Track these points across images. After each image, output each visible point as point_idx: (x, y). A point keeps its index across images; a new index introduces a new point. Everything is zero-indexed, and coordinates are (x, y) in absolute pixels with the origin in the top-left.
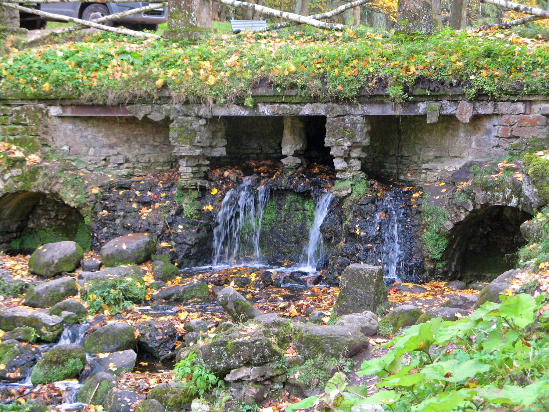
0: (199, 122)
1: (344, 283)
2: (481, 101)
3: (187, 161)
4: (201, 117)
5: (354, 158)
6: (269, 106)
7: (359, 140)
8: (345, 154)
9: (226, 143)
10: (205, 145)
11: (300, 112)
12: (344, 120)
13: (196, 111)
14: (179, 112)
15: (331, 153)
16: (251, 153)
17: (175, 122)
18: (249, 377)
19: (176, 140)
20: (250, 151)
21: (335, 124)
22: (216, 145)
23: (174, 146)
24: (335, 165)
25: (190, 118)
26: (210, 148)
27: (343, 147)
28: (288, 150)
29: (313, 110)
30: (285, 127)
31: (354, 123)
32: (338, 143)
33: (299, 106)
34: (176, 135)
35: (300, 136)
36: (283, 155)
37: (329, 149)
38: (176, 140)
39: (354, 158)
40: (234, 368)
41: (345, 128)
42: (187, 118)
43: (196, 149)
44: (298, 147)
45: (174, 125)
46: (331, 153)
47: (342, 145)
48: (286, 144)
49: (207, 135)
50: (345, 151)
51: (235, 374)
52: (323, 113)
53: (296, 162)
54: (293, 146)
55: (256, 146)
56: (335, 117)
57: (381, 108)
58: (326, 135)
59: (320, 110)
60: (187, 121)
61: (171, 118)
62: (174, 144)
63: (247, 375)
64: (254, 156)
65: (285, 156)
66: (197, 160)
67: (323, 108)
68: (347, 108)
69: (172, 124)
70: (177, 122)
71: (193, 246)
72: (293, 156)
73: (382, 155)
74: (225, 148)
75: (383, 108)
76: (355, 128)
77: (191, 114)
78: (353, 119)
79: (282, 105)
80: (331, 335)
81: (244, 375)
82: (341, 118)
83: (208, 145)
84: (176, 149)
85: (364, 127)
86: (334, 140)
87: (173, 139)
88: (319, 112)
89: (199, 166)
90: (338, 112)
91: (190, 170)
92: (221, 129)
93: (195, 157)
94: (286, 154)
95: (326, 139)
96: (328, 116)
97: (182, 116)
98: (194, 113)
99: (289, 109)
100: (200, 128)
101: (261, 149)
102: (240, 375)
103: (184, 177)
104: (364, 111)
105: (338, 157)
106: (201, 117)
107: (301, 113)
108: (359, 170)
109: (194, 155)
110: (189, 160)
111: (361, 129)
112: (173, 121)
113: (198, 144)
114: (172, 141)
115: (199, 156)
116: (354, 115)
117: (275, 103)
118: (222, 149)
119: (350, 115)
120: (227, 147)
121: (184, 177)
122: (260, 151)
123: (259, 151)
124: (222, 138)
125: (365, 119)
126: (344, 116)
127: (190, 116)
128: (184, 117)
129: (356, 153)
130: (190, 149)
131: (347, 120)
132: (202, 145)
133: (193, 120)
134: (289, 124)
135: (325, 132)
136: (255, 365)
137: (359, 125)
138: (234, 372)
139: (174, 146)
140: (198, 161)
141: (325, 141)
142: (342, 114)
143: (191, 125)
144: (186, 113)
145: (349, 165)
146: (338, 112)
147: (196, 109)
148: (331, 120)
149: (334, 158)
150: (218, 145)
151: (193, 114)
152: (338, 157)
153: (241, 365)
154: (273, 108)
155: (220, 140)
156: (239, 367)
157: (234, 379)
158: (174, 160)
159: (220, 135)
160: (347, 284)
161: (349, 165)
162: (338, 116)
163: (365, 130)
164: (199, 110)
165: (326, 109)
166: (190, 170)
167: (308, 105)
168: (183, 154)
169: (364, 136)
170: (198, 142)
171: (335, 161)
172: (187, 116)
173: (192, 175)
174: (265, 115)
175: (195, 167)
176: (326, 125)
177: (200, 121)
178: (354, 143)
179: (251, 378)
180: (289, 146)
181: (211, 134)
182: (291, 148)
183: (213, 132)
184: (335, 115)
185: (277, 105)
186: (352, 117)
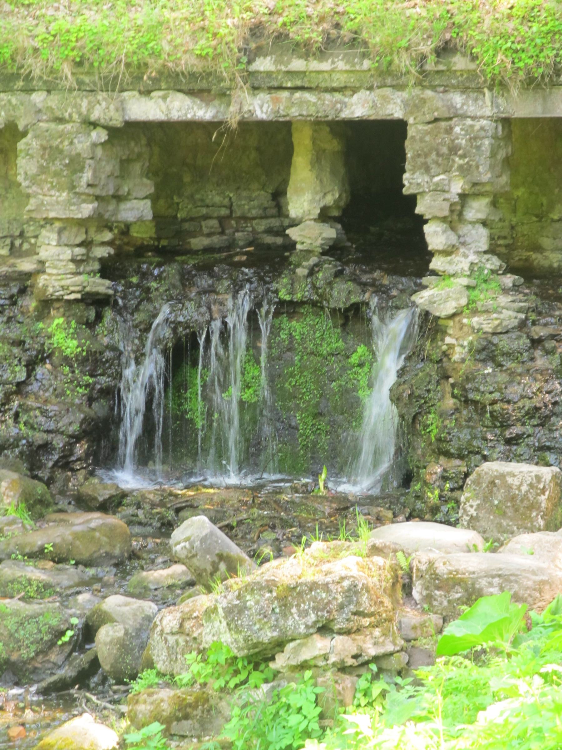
0: (89, 135)
1: (472, 506)
2: (321, 181)
3: (60, 232)
4: (94, 125)
5: (473, 223)
6: (263, 96)
7: (486, 177)
8: (452, 211)
9: (152, 190)
10: (104, 194)
11: (341, 110)
12: (449, 131)
13: (84, 110)
14: (40, 111)
15: (419, 210)
16: (206, 217)
17: (29, 136)
18: (326, 657)
19: (34, 180)
20: (204, 211)
21: (427, 138)
22: (129, 193)
23: (28, 196)
24: (428, 239)
25: (69, 126)
26: (114, 201)
27: (447, 196)
28: (306, 206)
29: (374, 106)
30: (296, 149)
31: (475, 138)
32: (437, 184)
33: (338, 96)
34: (33, 169)
35: (333, 172)
36: (293, 220)
37: (412, 200)
38: (34, 180)
39: (473, 223)
40: (293, 640)
41: (454, 150)
42: (61, 127)
43: (84, 201)
44: (329, 200)
45: (27, 144)
46: (419, 210)
47: (444, 191)
48: (299, 192)
49: (108, 168)
50: (451, 205)
51: (296, 651)
52: (398, 114)
53: (324, 235)
54: (317, 198)
55: (217, 199)
56: (429, 123)
57: (541, 101)
58: (407, 166)
59: (391, 106)
60: (61, 135)
61: (21, 128)
62: (30, 191)
63: (322, 652)
64: (214, 223)
65: (294, 224)
66: (84, 230)
67: (399, 101)
68: (457, 99)
69: (24, 140)
70: (36, 137)
71: (77, 438)
72: (315, 220)
73: (534, 219)
74: (148, 203)
75: (545, 99)
76: (478, 148)
77: (70, 116)
78: (472, 126)
79: (298, 95)
80: (500, 569)
81: (316, 653)
82: (443, 124)
83: (111, 193)
84: (32, 201)
85: (499, 147)
86: (427, 178)
87: (25, 179)
88: (388, 112)
89: (86, 244)
90: (437, 109)
91: (67, 253)
92: (139, 156)
93: (82, 223)
94: (300, 215)
95: (406, 176)
96: (411, 121)
97: (47, 121)
98: (80, 114)
99: (315, 104)
100: (93, 152)
101: (230, 207)
102: (306, 655)
103: (54, 271)
104: (498, 107)
105: (435, 218)
106: (94, 125)
107: (345, 114)
108: (485, 252)
109: (79, 216)
110: (64, 228)
111: (492, 151)
112: (24, 134)
113: (91, 191)
114: (25, 184)
115: (89, 218)
116: (473, 118)
117: (280, 88)
118: (142, 203)
119: (464, 117)
120: (154, 199)
121: (54, 271)
122: (227, 212)
123: (224, 212)
124: (142, 175)
125: (500, 128)
126: (450, 119)
127: (68, 122)
128: (53, 126)
129: (478, 211)
130: (69, 203)
131: (457, 129)
132: (97, 192)
133: (78, 132)
134: (308, 142)
135: (403, 158)
136: (340, 633)
137: (487, 142)
138: (294, 648)
139: (28, 196)
140: (86, 233)
141: (406, 182)
142: (447, 115)
143: (71, 143)
144: (58, 114)
145: (462, 240)
146: (437, 109)
147: (84, 104)
148: (418, 131)
149: (426, 222)
150: (134, 195)
151: (75, 116)
152: (435, 218)
153: (311, 631)
154: (276, 101)
155: (138, 181)
156: (307, 636)
157: (294, 663)
158: (17, 233)
159: (137, 168)
160: (479, 507)
161: (462, 240)
162: (436, 120)
163: (502, 155)
164: (90, 108)
165: (405, 103)
166: (67, 253)
167: (363, 94)
168: (52, 215)
169: (498, 169)
170: (89, 185)
171: (427, 229)
172: (60, 120)
173: (72, 266)
174: (254, 118)
175: (78, 246)
176: (407, 143)
177: (94, 134)
178: (475, 184)
179: (333, 659)
180: (307, 196)
181: (117, 167)
182: (311, 201)
183: (122, 162)
184: (428, 118)
185: (285, 94)
186: (469, 122)
